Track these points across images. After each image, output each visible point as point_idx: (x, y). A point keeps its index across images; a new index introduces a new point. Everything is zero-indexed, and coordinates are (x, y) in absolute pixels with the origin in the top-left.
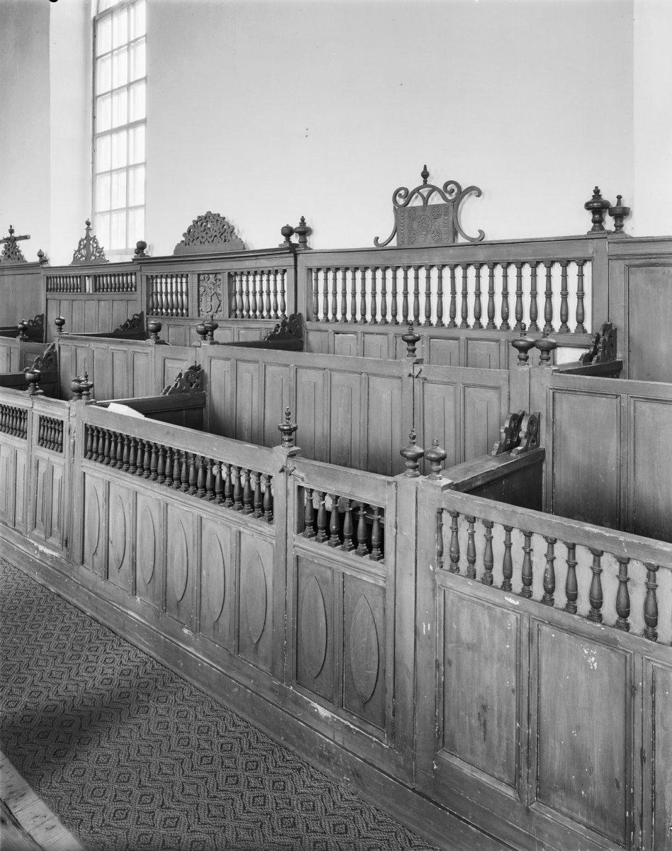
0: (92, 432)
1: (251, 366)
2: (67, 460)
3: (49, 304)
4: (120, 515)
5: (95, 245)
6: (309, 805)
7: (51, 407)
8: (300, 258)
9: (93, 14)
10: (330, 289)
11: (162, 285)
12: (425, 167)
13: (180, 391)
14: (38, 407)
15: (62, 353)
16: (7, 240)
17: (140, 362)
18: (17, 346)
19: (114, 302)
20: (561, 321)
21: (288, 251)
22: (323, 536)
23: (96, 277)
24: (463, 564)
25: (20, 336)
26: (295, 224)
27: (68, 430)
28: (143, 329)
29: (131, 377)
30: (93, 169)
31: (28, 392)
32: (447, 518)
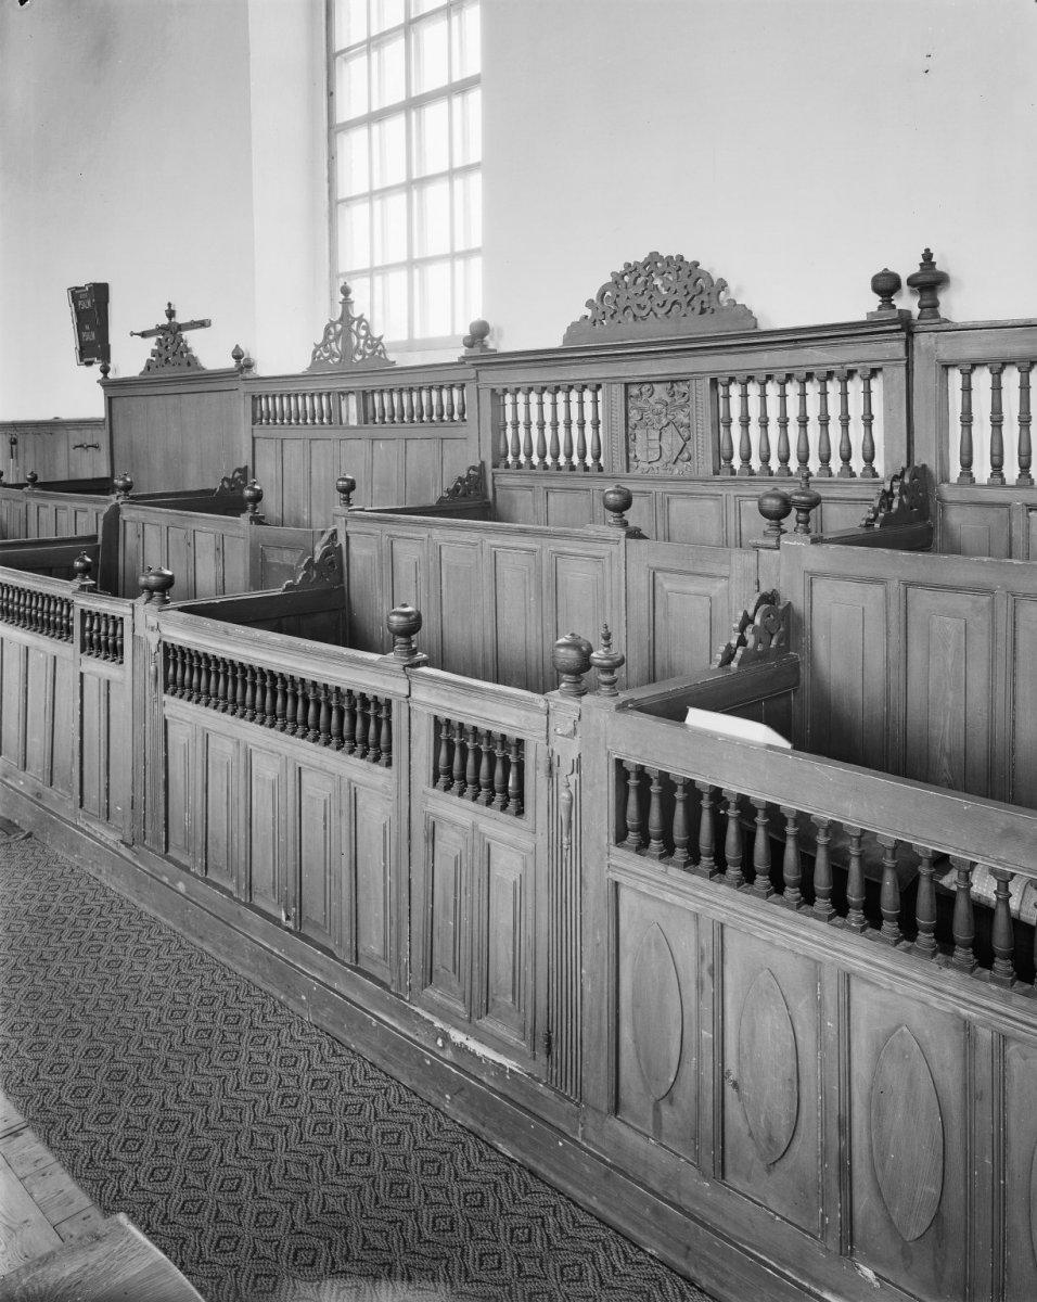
0: (633, 783)
2: (542, 841)
5: (363, 333)
6: (523, 1233)
7: (476, 701)
11: (518, 408)
12: (169, 305)
15: (352, 547)
16: (162, 329)
18: (241, 533)
19: (409, 442)
20: (865, 459)
21: (899, 327)
22: (861, 922)
23: (365, 395)
25: (251, 514)
27: (543, 766)
28: (486, 496)
29: (548, 606)
30: (331, 191)
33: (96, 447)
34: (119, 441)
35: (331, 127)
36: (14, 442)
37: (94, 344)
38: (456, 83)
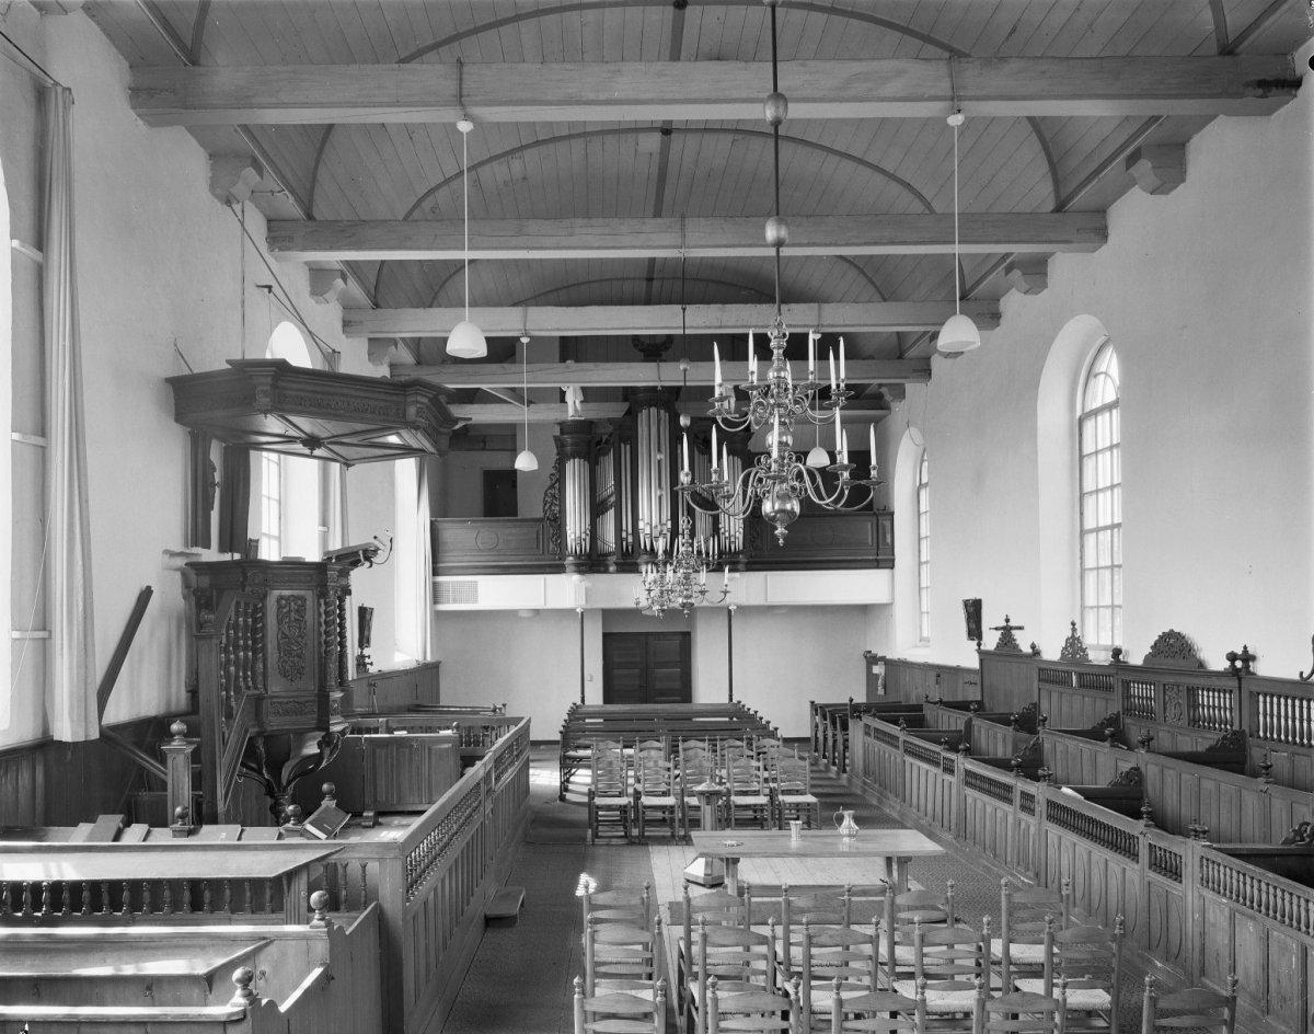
0: (1050, 804)
1: (1171, 772)
3: (579, 694)
4: (1066, 855)
9: (1079, 413)
10: (1283, 714)
11: (1136, 689)
13: (1121, 784)
14: (1021, 785)
17: (1101, 759)
24: (1210, 884)
26: (1239, 651)
32: (1205, 861)
34: (986, 683)
35: (1081, 531)
37: (975, 632)
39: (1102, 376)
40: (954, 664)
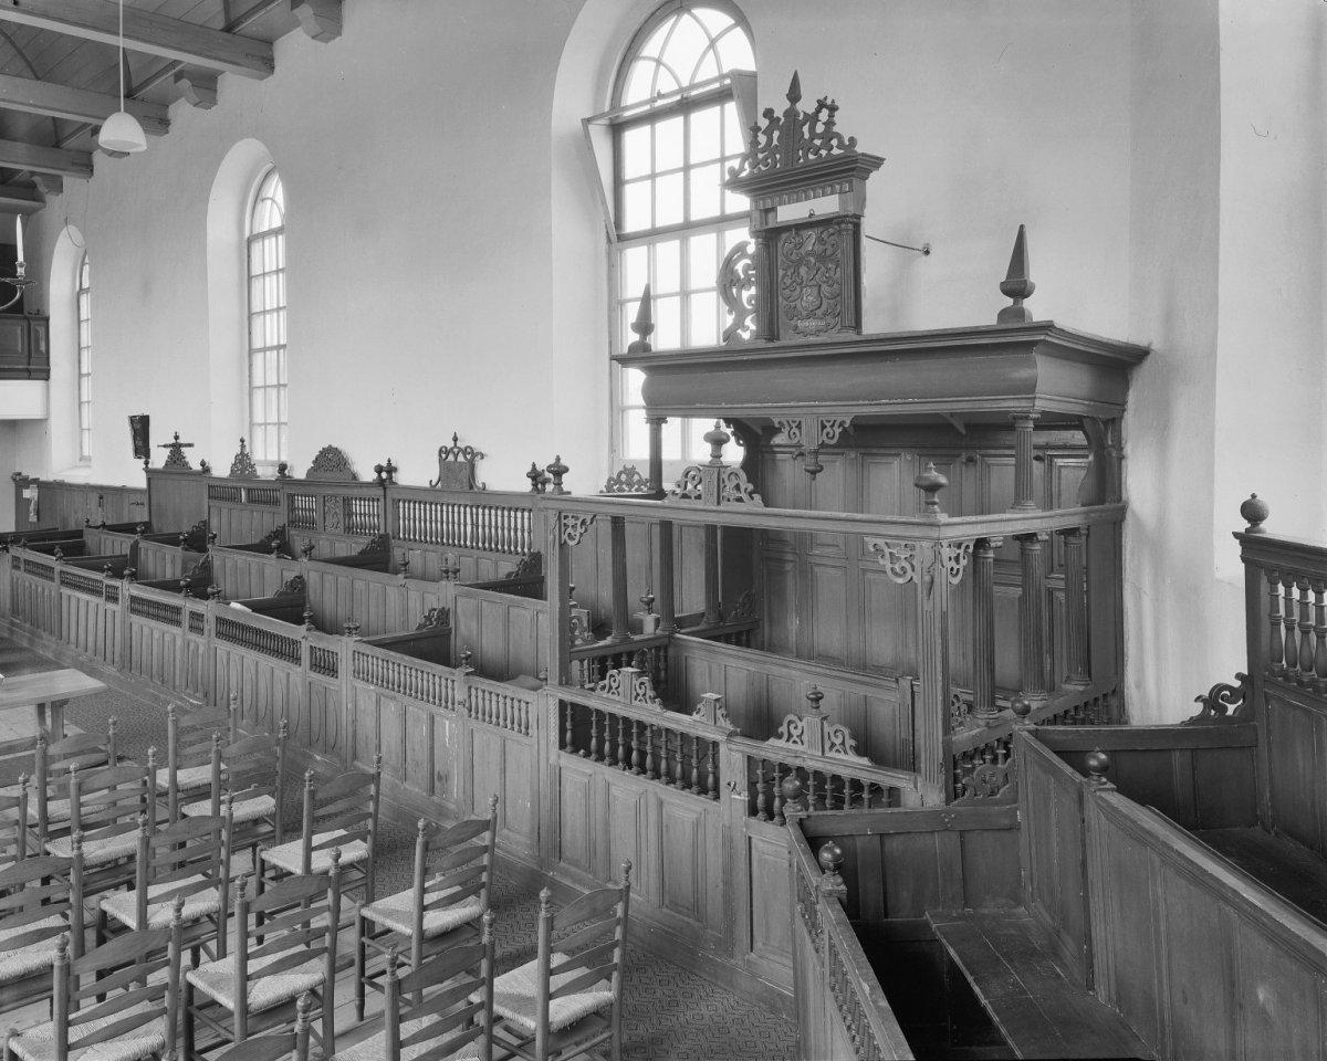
0: (220, 621)
8: (388, 492)
11: (300, 502)
14: (189, 605)
23: (249, 490)
26: (384, 464)
31: (183, 594)
33: (142, 504)
35: (250, 350)
36: (101, 498)
37: (142, 449)
38: (732, 17)
39: (269, 202)
40: (118, 483)
